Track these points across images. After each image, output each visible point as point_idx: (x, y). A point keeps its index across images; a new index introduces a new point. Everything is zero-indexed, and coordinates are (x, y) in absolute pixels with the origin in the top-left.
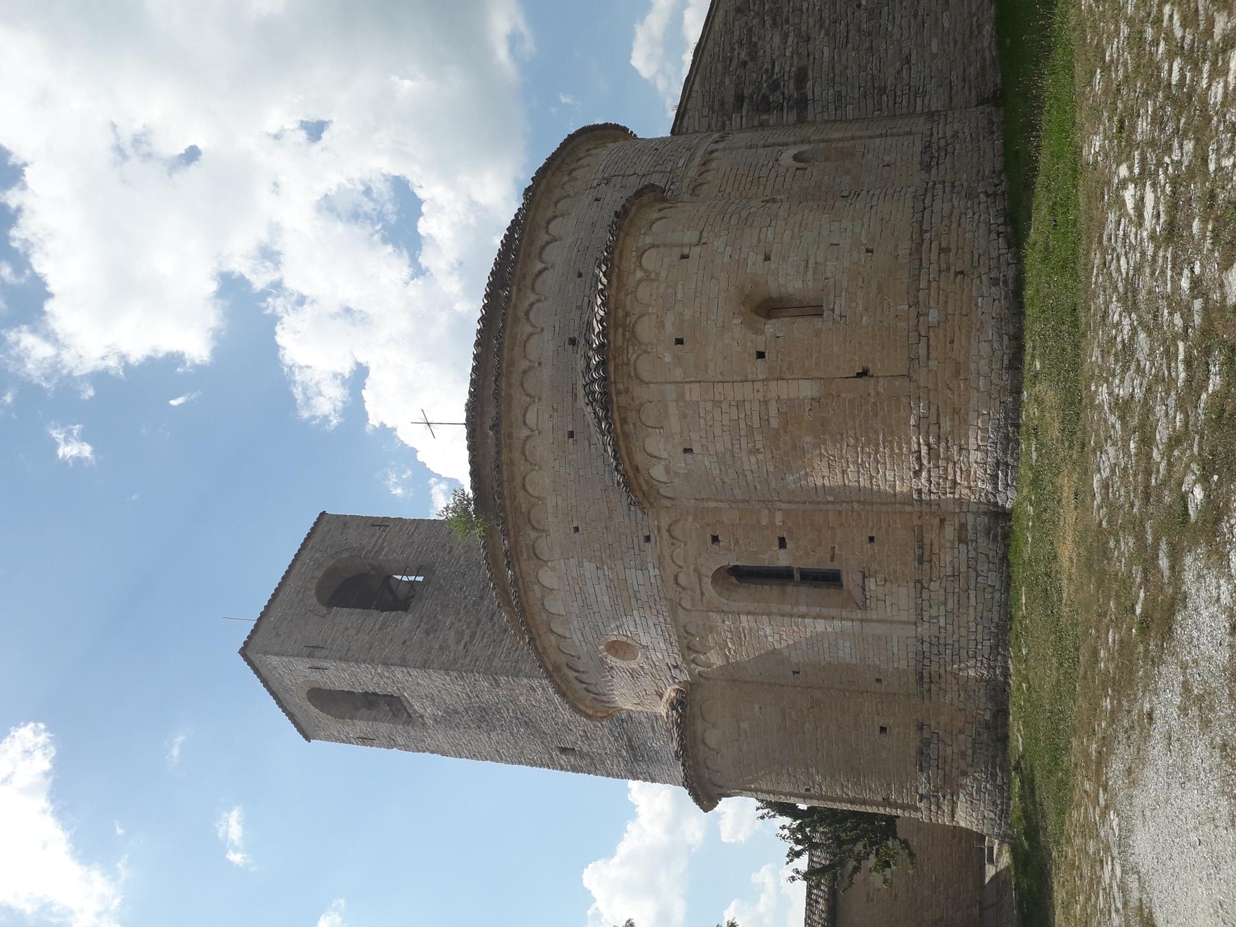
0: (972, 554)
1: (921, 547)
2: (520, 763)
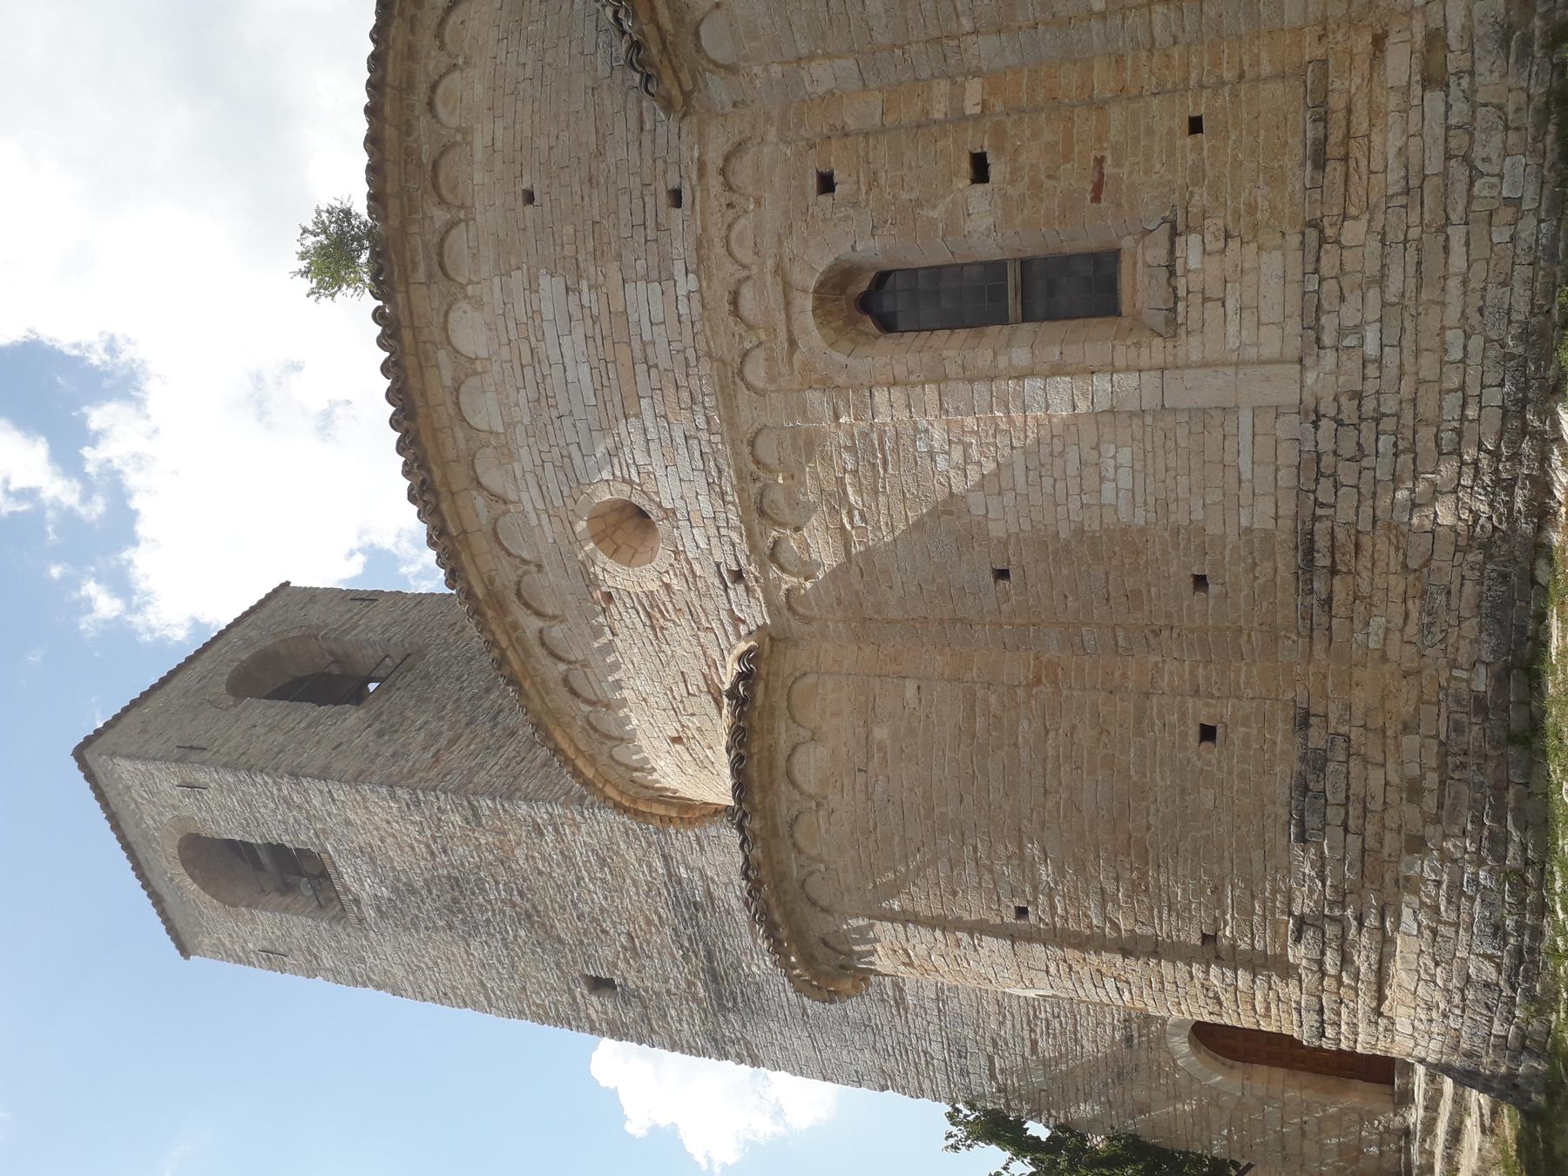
0: (1460, 108)
1: (1323, 119)
2: (521, 1014)
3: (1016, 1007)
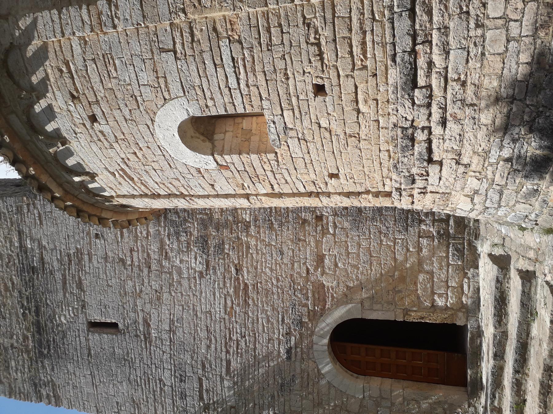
3: (218, 331)
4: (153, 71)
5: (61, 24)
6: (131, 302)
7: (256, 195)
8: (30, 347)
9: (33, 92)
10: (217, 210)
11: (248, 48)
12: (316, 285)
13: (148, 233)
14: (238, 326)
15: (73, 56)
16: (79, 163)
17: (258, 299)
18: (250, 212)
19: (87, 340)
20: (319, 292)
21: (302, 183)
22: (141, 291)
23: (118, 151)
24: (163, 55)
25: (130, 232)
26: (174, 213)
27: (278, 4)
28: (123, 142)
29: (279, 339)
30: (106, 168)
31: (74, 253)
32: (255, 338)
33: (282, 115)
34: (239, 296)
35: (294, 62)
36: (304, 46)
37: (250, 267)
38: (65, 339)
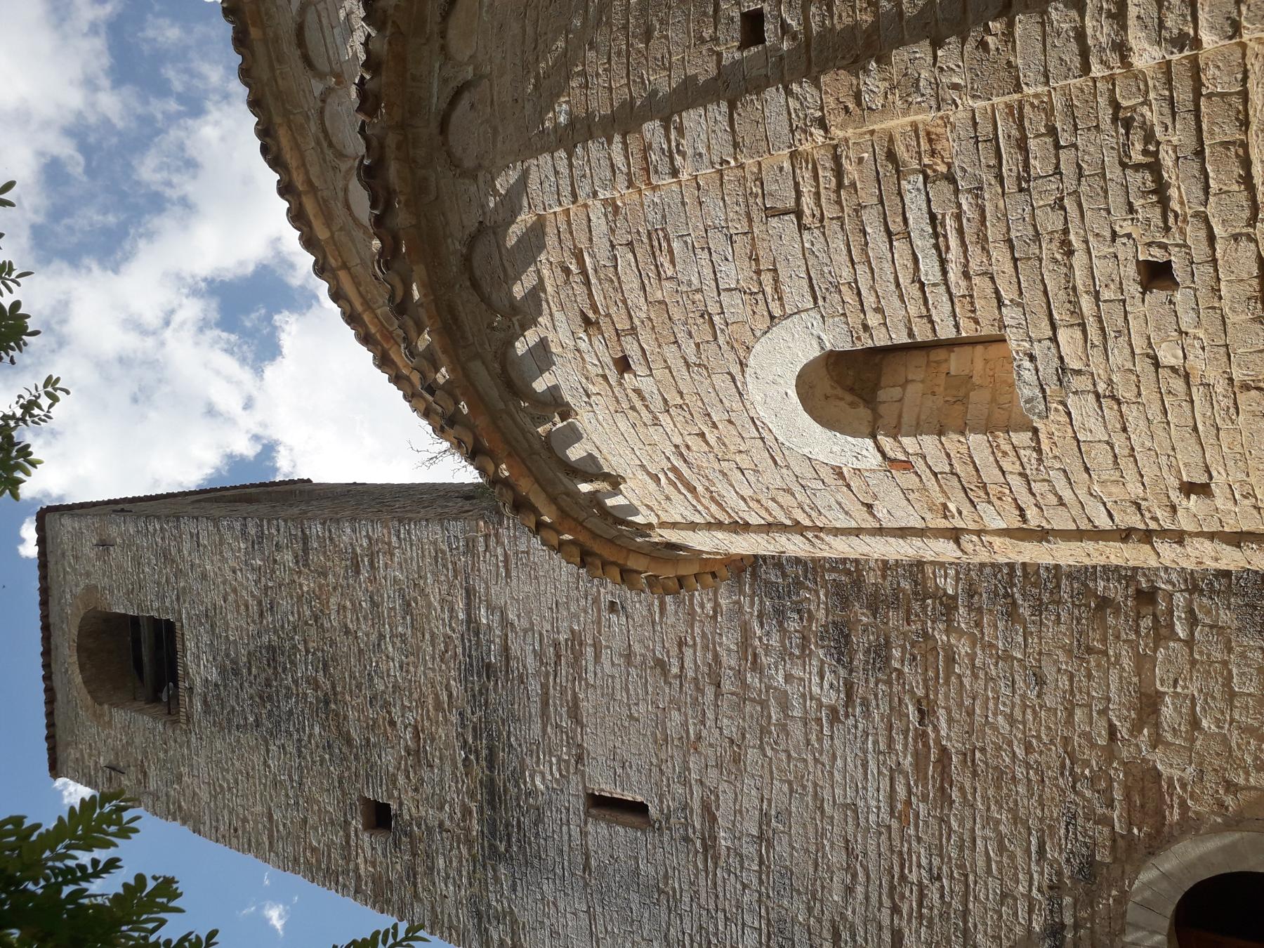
3: (873, 855)
4: (750, 258)
5: (572, 177)
6: (678, 761)
7: (979, 533)
8: (475, 833)
9: (515, 315)
10: (872, 564)
11: (969, 191)
12: (1134, 771)
13: (716, 606)
14: (922, 851)
15: (591, 240)
16: (590, 455)
17: (975, 789)
18: (957, 573)
19: (584, 834)
20: (1143, 788)
21: (1104, 504)
22: (699, 738)
23: (668, 430)
24: (774, 222)
25: (680, 603)
26: (774, 565)
27: (1047, 83)
28: (679, 411)
29: (1028, 897)
30: (642, 466)
31: (566, 640)
32: (967, 886)
33: (1054, 339)
34: (926, 778)
35: (1088, 214)
36: (1114, 172)
37: (954, 708)
38: (541, 826)
